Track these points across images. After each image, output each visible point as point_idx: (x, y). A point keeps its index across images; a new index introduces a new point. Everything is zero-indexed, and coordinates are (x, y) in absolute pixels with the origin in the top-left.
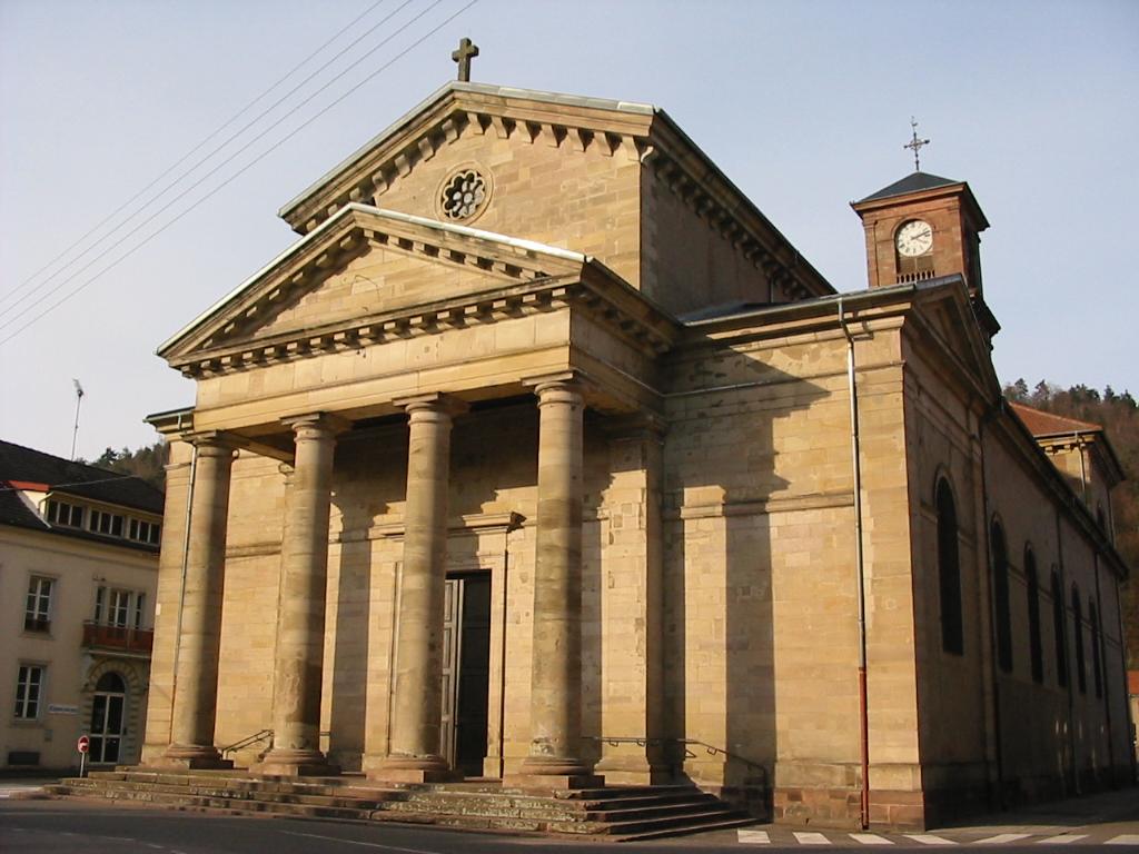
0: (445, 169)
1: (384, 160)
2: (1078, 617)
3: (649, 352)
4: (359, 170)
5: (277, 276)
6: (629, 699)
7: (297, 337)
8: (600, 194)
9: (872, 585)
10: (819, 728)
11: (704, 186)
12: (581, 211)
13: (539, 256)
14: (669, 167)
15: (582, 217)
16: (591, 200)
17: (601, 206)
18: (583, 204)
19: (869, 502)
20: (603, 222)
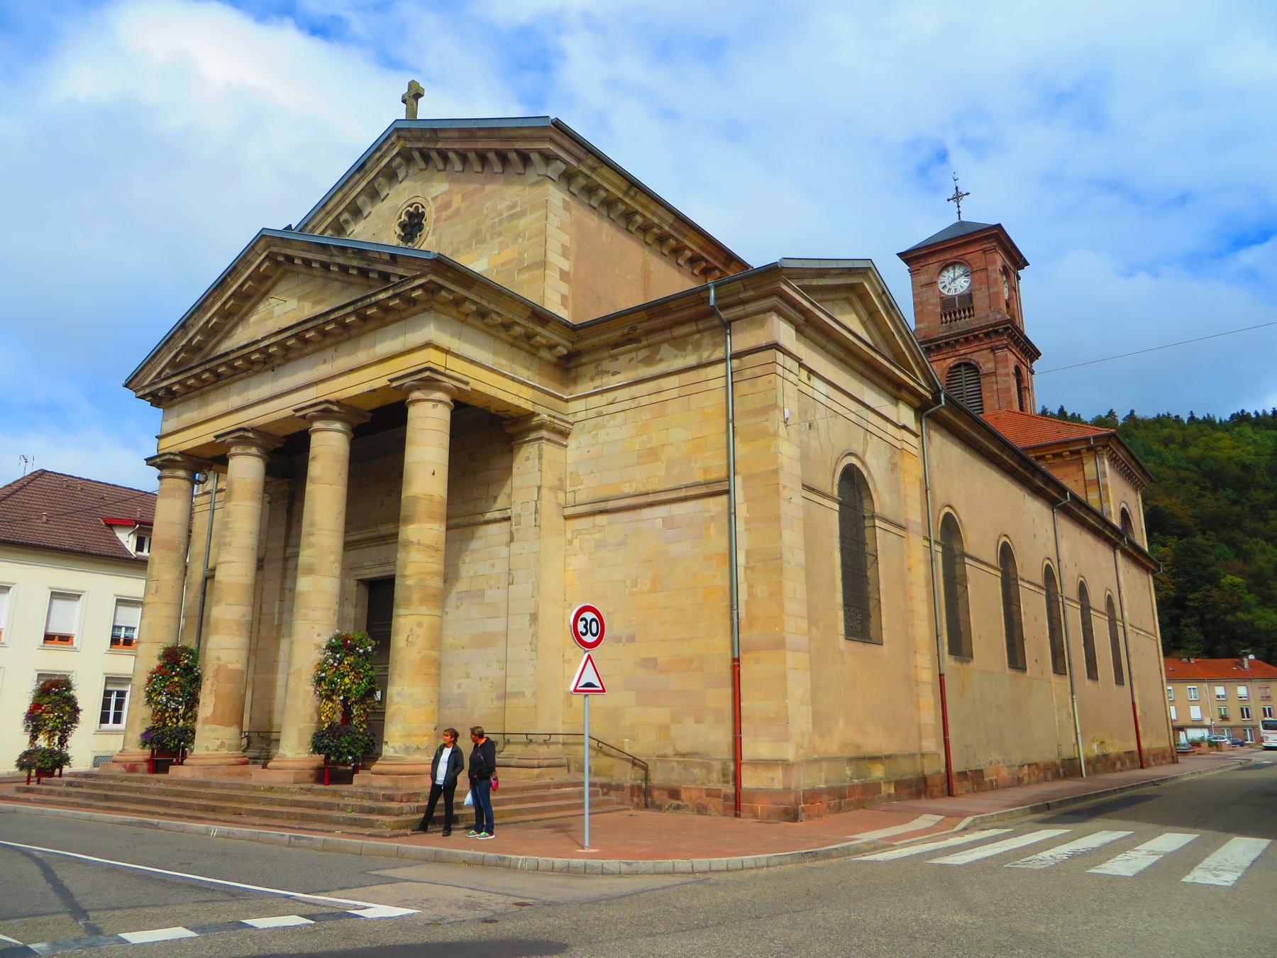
0: (397, 205)
1: (347, 201)
2: (1086, 609)
3: (544, 354)
4: (328, 213)
5: (212, 304)
6: (523, 694)
7: (224, 360)
8: (514, 211)
9: (745, 572)
10: (697, 722)
11: (627, 200)
12: (498, 229)
13: (399, 259)
14: (581, 181)
15: (500, 234)
16: (507, 217)
17: (515, 222)
18: (501, 222)
19: (744, 488)
20: (519, 235)
